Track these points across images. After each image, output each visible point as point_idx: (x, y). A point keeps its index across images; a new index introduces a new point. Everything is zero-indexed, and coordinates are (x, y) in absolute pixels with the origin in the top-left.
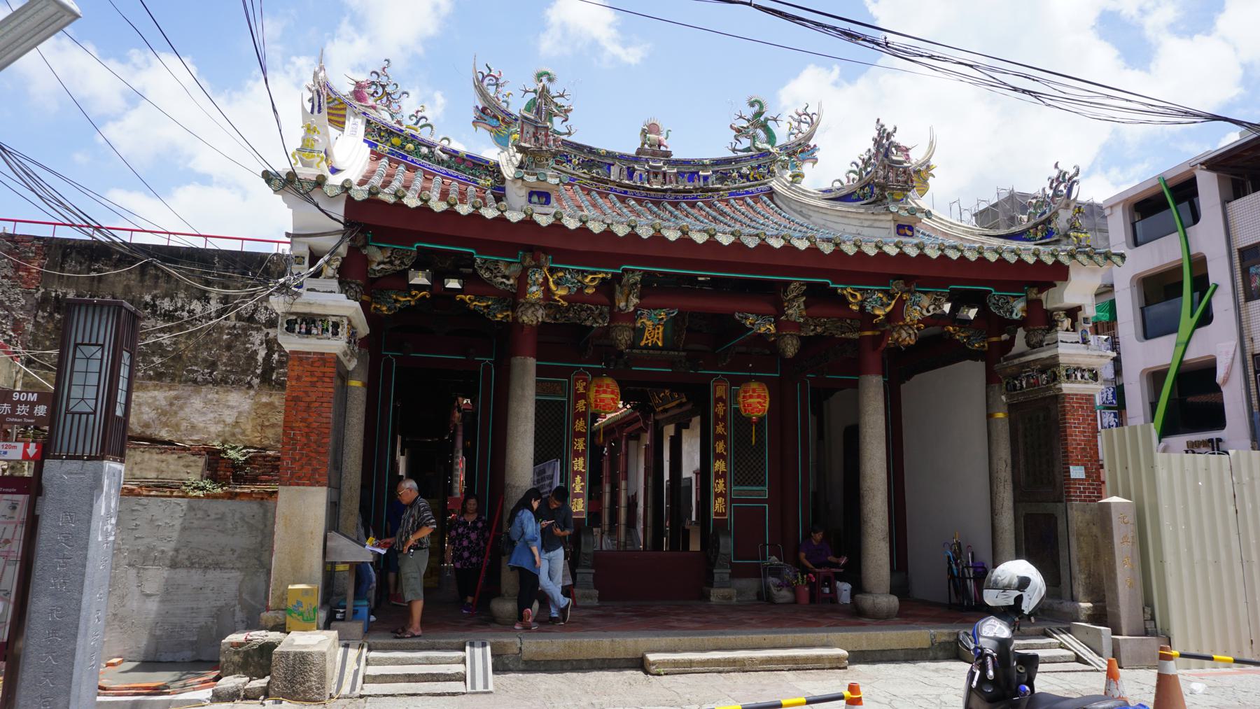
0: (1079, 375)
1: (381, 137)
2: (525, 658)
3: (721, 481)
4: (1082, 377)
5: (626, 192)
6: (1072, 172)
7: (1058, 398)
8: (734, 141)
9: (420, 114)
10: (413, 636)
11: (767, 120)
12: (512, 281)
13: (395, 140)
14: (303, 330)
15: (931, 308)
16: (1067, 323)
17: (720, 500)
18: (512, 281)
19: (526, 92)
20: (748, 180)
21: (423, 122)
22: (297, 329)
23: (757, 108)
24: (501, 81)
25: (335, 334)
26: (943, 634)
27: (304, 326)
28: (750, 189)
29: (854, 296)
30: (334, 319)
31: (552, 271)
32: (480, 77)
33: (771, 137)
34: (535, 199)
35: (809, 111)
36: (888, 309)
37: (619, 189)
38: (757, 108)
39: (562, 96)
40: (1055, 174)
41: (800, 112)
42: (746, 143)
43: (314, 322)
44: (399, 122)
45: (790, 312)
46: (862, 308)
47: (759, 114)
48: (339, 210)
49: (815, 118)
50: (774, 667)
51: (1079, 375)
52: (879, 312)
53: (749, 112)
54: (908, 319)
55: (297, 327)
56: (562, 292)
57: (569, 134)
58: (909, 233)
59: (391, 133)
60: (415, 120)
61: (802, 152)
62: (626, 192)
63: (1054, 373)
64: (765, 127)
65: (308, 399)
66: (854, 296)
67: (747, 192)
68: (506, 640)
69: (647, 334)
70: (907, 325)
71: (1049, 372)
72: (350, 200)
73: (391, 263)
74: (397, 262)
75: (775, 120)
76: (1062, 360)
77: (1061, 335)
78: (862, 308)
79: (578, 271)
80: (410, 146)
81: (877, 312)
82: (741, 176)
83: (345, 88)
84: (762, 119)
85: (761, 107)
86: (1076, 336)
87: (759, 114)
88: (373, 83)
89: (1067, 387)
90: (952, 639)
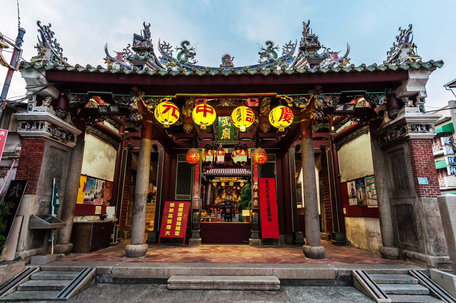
0: (419, 128)
2: (113, 277)
3: (256, 193)
4: (422, 129)
6: (408, 28)
7: (407, 140)
8: (260, 59)
10: (129, 254)
11: (273, 49)
14: (29, 128)
15: (331, 102)
17: (256, 201)
19: (178, 49)
23: (270, 45)
25: (42, 128)
26: (342, 271)
31: (145, 99)
32: (161, 46)
33: (276, 55)
35: (291, 43)
36: (307, 104)
39: (192, 49)
40: (398, 33)
41: (288, 44)
42: (265, 59)
45: (263, 112)
47: (271, 47)
49: (294, 46)
51: (419, 128)
53: (266, 47)
57: (195, 63)
61: (288, 59)
63: (404, 129)
64: (273, 51)
65: (29, 156)
66: (289, 100)
69: (223, 134)
71: (401, 129)
73: (77, 100)
75: (277, 48)
77: (407, 109)
78: (294, 105)
81: (301, 106)
83: (114, 55)
87: (271, 47)
88: (124, 53)
89: (412, 135)
90: (348, 274)
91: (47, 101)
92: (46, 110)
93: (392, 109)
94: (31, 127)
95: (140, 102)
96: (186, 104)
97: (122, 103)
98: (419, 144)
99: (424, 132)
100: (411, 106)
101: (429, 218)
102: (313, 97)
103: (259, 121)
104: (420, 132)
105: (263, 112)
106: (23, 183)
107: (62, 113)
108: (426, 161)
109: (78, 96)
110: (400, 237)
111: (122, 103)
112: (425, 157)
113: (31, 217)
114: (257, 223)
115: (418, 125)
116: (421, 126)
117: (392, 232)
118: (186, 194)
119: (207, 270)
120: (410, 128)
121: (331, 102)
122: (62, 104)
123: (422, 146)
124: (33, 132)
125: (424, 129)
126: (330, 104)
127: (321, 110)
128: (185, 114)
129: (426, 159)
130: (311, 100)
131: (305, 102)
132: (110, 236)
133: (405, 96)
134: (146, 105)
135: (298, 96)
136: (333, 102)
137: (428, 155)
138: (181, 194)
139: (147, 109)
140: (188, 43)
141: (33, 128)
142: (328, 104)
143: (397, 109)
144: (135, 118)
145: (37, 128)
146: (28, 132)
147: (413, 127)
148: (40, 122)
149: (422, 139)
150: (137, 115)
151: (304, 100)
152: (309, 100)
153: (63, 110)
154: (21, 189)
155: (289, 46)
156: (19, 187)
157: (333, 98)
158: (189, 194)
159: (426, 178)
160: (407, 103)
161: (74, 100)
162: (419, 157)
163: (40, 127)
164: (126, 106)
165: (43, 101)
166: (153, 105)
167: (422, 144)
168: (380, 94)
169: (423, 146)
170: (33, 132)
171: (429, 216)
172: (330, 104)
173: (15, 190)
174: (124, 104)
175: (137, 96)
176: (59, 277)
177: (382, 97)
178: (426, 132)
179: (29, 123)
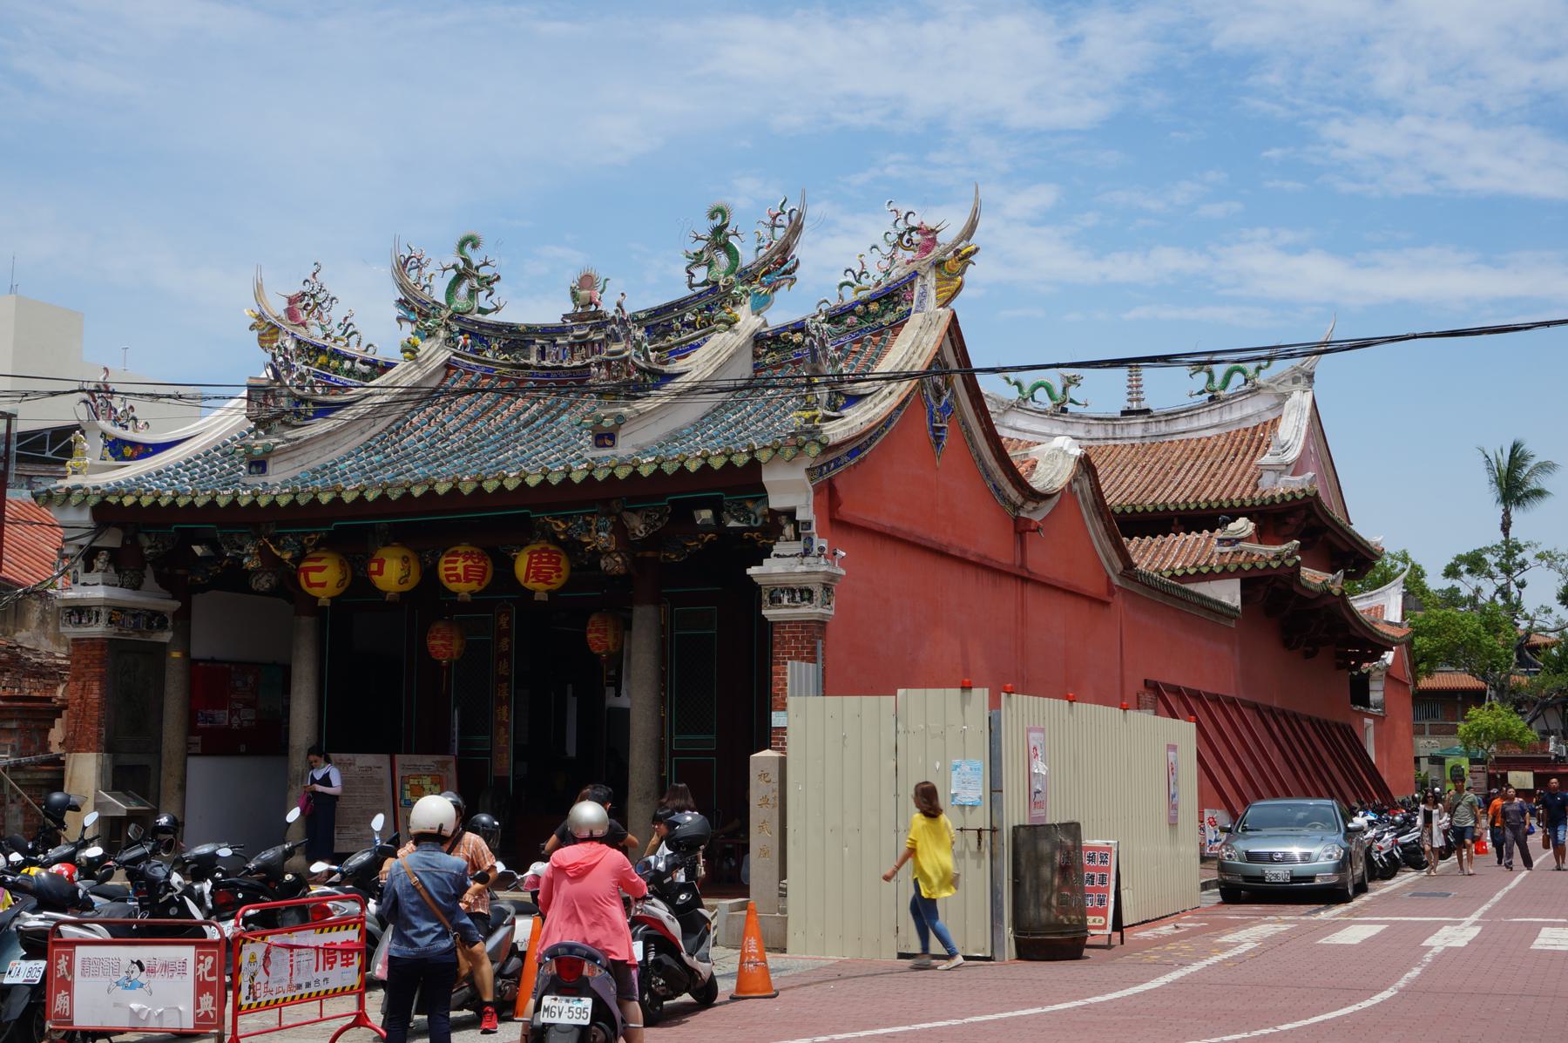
4: (793, 599)
7: (767, 627)
13: (322, 359)
58: (608, 442)
59: (320, 350)
86: (798, 547)
87: (719, 230)
95: (264, 552)
116: (793, 591)
169: (796, 638)
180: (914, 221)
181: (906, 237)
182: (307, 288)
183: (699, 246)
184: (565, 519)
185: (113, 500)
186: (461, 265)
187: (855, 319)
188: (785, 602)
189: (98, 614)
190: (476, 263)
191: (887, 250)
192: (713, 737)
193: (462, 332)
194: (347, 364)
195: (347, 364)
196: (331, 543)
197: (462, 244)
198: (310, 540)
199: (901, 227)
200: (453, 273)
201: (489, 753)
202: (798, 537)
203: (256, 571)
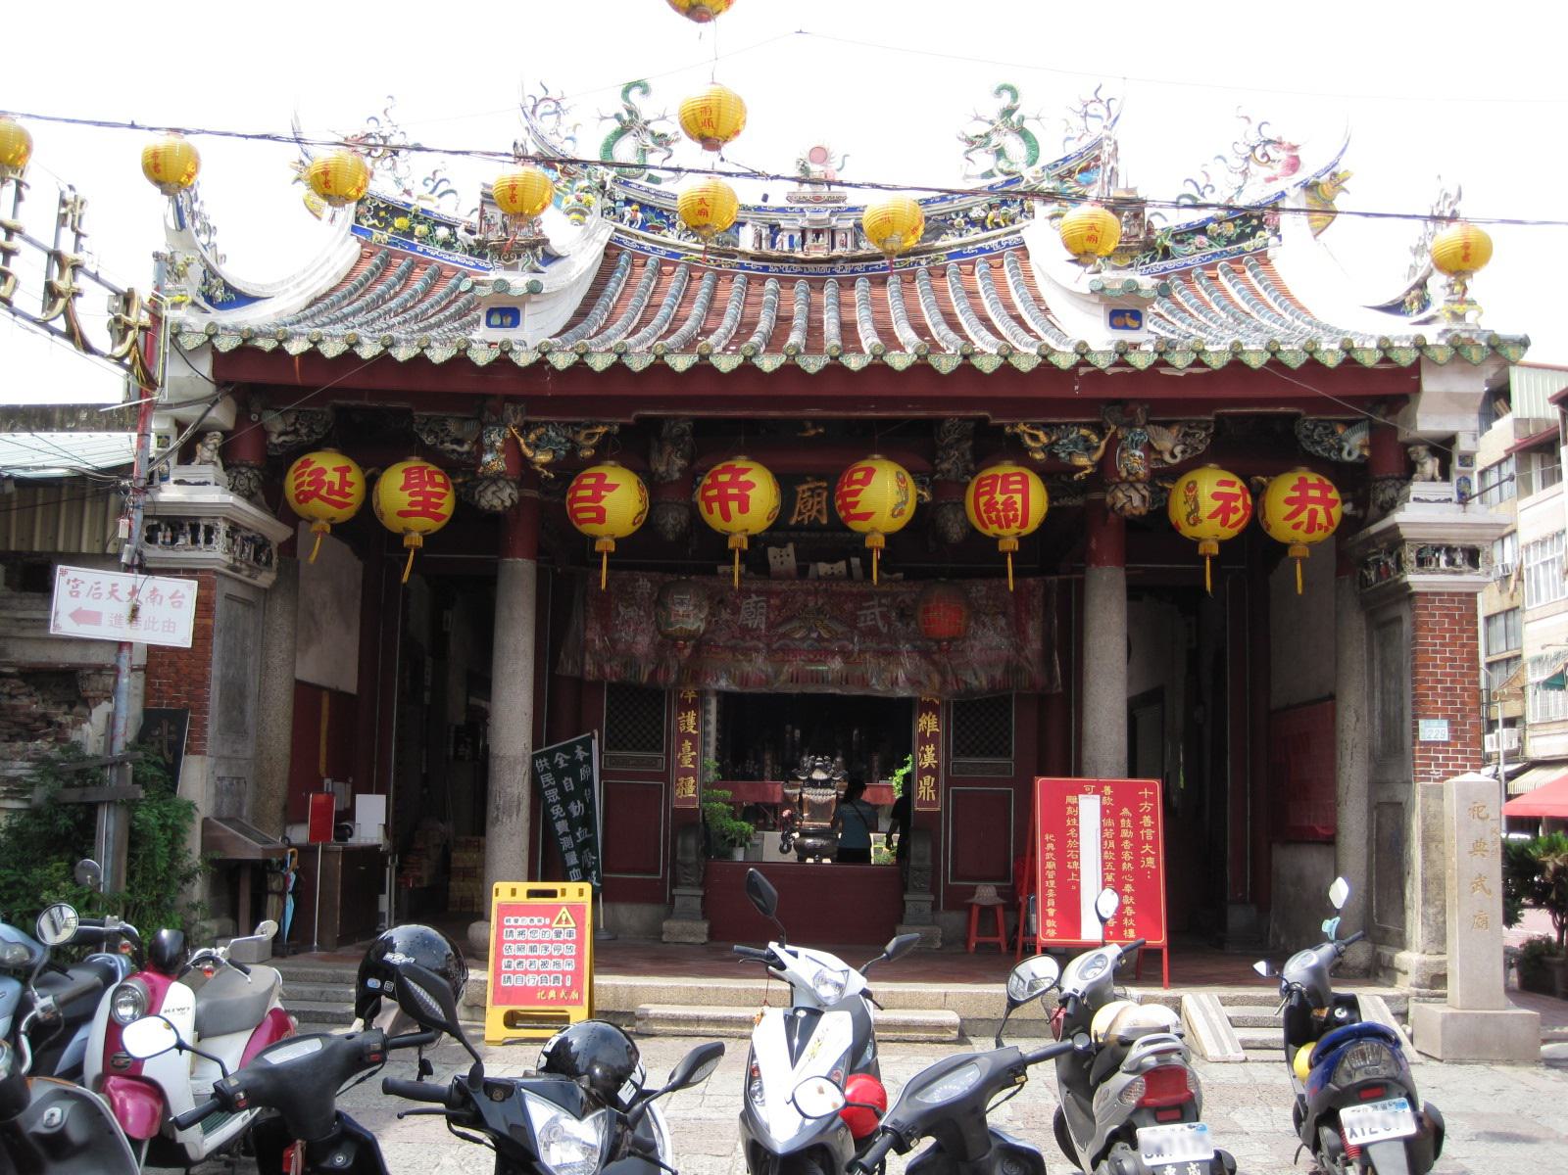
1: (381, 220)
3: (930, 749)
4: (1451, 562)
5: (766, 269)
7: (1405, 594)
9: (439, 176)
12: (466, 448)
13: (400, 222)
14: (168, 540)
15: (1178, 450)
16: (1431, 466)
18: (466, 448)
20: (984, 228)
21: (443, 187)
22: (160, 540)
23: (1006, 100)
24: (564, 105)
25: (208, 541)
27: (169, 534)
28: (984, 245)
29: (1035, 438)
30: (206, 522)
31: (526, 428)
34: (496, 320)
37: (754, 264)
38: (1007, 97)
43: (182, 526)
44: (407, 192)
45: (945, 466)
46: (1052, 455)
48: (205, 367)
50: (913, 1035)
51: (1443, 559)
52: (1082, 461)
53: (992, 108)
54: (1124, 474)
55: (160, 535)
56: (543, 457)
58: (1130, 322)
59: (395, 211)
60: (431, 185)
62: (766, 269)
66: (1035, 438)
67: (981, 250)
68: (344, 971)
70: (1124, 481)
72: (215, 352)
73: (296, 432)
74: (304, 431)
76: (1405, 532)
77: (1417, 488)
78: (1052, 455)
79: (567, 425)
80: (421, 229)
82: (973, 223)
84: (1015, 118)
85: (1015, 96)
86: (1449, 489)
87: (1008, 112)
91: (211, 447)
92: (211, 479)
93: (1383, 480)
94: (174, 540)
95: (512, 445)
96: (665, 430)
97: (448, 446)
98: (1440, 608)
99: (1455, 573)
100: (1433, 479)
101: (1433, 846)
102: (1115, 434)
103: (933, 493)
104: (1444, 572)
105: (945, 466)
106: (177, 718)
107: (249, 479)
108: (1451, 667)
109: (297, 419)
110: (1378, 904)
111: (448, 446)
112: (1451, 652)
113: (205, 820)
114: (928, 863)
115: (1438, 550)
116: (1450, 550)
117: (1362, 893)
118: (643, 748)
119: (746, 990)
120: (1413, 556)
121: (1178, 450)
122: (247, 453)
123: (1447, 616)
124: (184, 554)
125: (1459, 561)
126: (1173, 456)
127: (1139, 481)
128: (662, 469)
129: (1455, 660)
130: (1107, 446)
131: (1089, 449)
132: (376, 903)
133: (1419, 442)
134: (529, 453)
135: (1066, 424)
136: (1183, 452)
137: (1463, 645)
138: (625, 747)
139: (534, 463)
140: (644, 87)
141: (181, 541)
142: (1167, 457)
143: (1398, 479)
144: (496, 502)
145: (195, 541)
146: (171, 554)
147: (1423, 555)
148: (203, 523)
149: (1449, 594)
150: (501, 490)
151: (1086, 439)
152: (1103, 443)
153: (251, 468)
154: (174, 737)
155: (1091, 109)
156: (170, 733)
157: (1186, 435)
158: (656, 746)
159: (1445, 723)
160: (1422, 465)
161: (285, 433)
162: (1434, 652)
163: (202, 537)
164: (460, 454)
165: (199, 446)
166: (554, 451)
167: (1448, 608)
168: (1349, 424)
169: (1451, 617)
170: (184, 554)
171: (1433, 840)
172: (1173, 456)
173: (160, 742)
174: (455, 447)
175: (502, 423)
176: (322, 993)
177: (1354, 433)
178: (1461, 573)
179: (169, 524)
180: (1269, 133)
181: (1259, 152)
182: (372, 128)
183: (983, 128)
184: (1048, 428)
185: (268, 345)
186: (626, 117)
187: (1204, 239)
188: (1443, 564)
189: (209, 531)
190: (645, 115)
191: (1239, 163)
192: (1010, 761)
193: (628, 202)
194: (442, 232)
195: (442, 232)
196: (633, 447)
197: (626, 91)
198: (590, 436)
199: (1254, 139)
200: (616, 125)
201: (665, 776)
202: (1445, 474)
203: (496, 478)
